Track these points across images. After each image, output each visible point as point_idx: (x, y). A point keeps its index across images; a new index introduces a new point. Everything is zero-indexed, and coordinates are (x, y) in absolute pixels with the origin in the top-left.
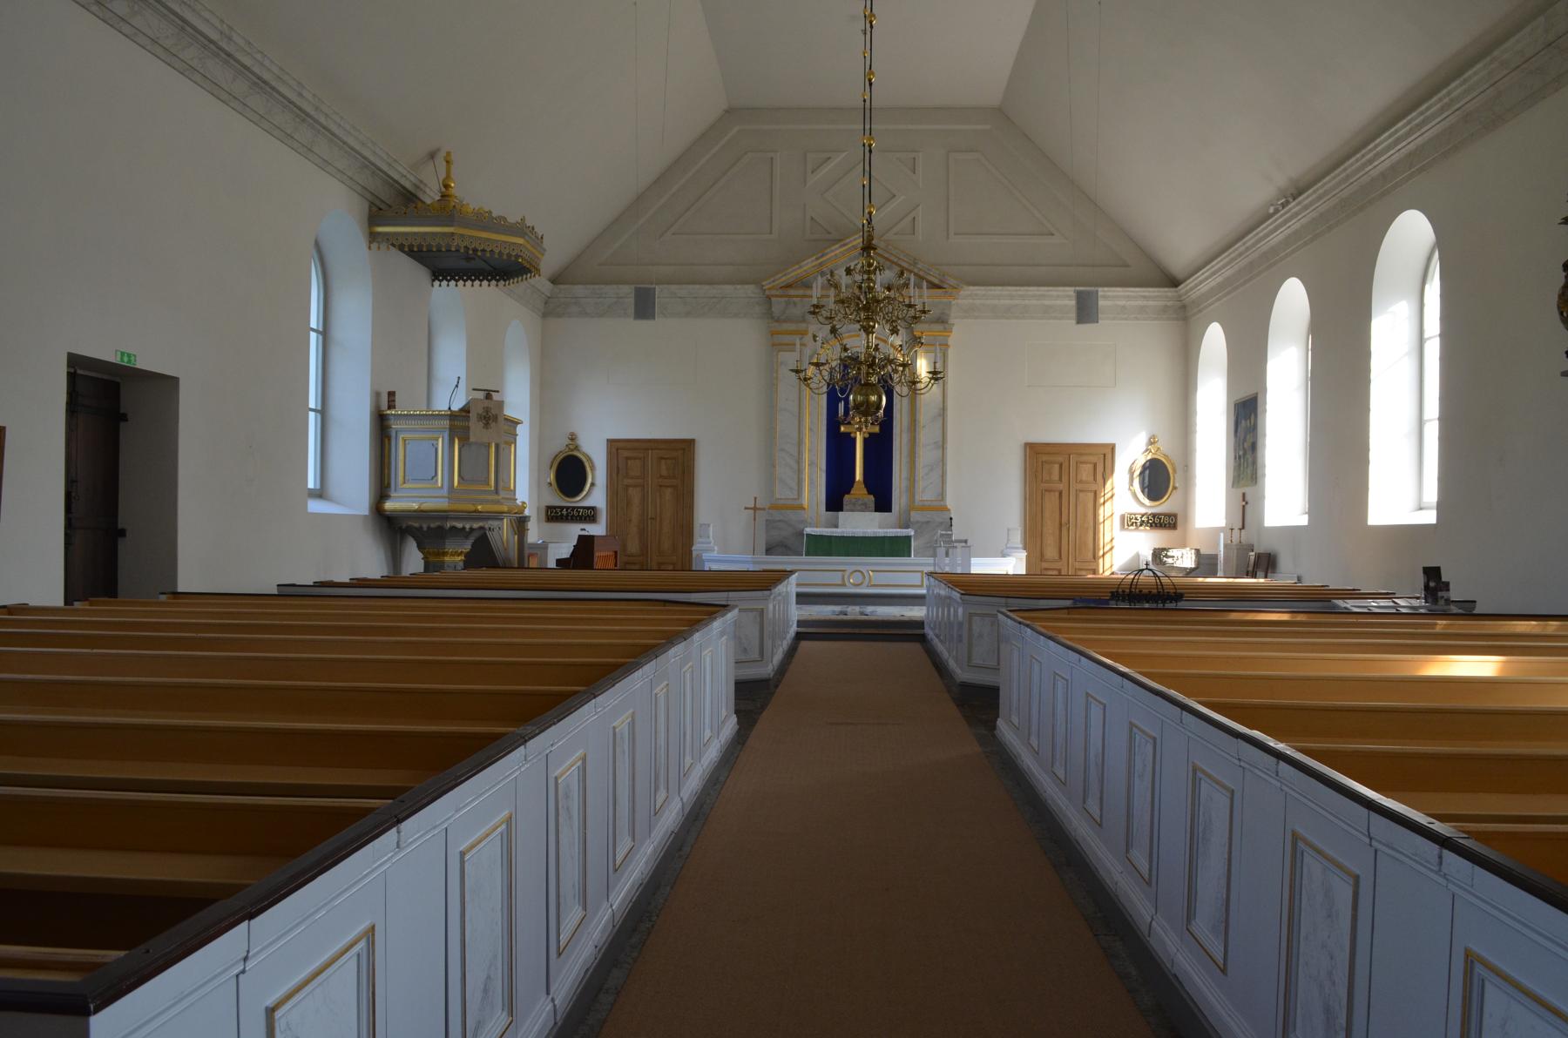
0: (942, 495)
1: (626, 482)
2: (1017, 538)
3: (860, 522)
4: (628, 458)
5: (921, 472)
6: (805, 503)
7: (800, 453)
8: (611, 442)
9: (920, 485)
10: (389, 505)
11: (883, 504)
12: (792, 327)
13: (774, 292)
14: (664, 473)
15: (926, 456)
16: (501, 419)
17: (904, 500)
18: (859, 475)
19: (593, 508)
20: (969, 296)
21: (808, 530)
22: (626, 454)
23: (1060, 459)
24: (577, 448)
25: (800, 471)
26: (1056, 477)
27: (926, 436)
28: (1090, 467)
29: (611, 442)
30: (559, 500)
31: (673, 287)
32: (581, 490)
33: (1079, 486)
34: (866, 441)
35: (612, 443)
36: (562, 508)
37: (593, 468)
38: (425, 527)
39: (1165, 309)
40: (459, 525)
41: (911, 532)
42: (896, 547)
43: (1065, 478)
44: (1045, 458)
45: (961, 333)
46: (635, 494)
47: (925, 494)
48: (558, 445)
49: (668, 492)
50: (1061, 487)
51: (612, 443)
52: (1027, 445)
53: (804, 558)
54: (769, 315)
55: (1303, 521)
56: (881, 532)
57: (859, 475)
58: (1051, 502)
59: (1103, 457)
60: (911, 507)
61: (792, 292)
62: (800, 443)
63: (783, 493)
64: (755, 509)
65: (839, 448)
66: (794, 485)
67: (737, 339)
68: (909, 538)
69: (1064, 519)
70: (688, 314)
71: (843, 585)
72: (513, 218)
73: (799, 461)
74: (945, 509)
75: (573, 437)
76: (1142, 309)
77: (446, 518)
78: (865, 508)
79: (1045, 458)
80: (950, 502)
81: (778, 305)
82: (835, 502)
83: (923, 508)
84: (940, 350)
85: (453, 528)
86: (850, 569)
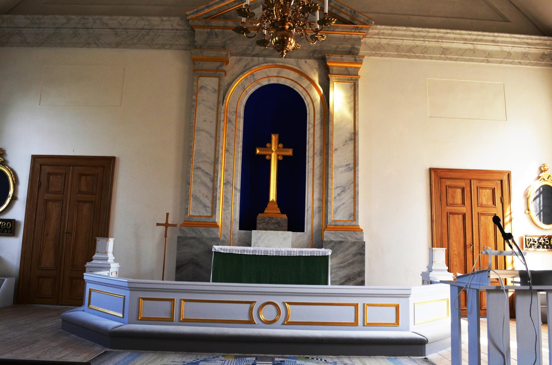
0: (354, 215)
1: (47, 196)
3: (274, 242)
4: (49, 174)
5: (333, 193)
6: (219, 220)
7: (215, 171)
8: (35, 158)
9: (333, 205)
11: (296, 224)
12: (213, 54)
13: (196, 22)
14: (84, 188)
15: (339, 177)
17: (316, 221)
18: (273, 196)
20: (377, 35)
21: (216, 248)
23: (462, 184)
25: (214, 189)
26: (459, 200)
27: (339, 158)
28: (489, 192)
29: (35, 158)
31: (105, 18)
33: (481, 210)
34: (279, 163)
39: (543, 57)
41: (329, 252)
42: (309, 271)
43: (467, 202)
44: (449, 183)
45: (366, 69)
46: (54, 209)
47: (338, 213)
49: (86, 208)
50: (463, 209)
52: (431, 170)
53: (211, 283)
54: (192, 45)
56: (296, 251)
57: (273, 196)
58: (456, 222)
59: (500, 183)
60: (324, 226)
61: (214, 23)
62: (216, 161)
63: (196, 211)
64: (166, 225)
65: (254, 173)
66: (208, 203)
67: (162, 70)
68: (325, 258)
69: (469, 242)
70: (118, 45)
71: (250, 322)
73: (214, 180)
74: (357, 230)
76: (525, 55)
78: (277, 227)
79: (449, 183)
80: (361, 223)
81: (200, 36)
82: (248, 222)
83: (337, 228)
84: (352, 79)
86: (260, 300)
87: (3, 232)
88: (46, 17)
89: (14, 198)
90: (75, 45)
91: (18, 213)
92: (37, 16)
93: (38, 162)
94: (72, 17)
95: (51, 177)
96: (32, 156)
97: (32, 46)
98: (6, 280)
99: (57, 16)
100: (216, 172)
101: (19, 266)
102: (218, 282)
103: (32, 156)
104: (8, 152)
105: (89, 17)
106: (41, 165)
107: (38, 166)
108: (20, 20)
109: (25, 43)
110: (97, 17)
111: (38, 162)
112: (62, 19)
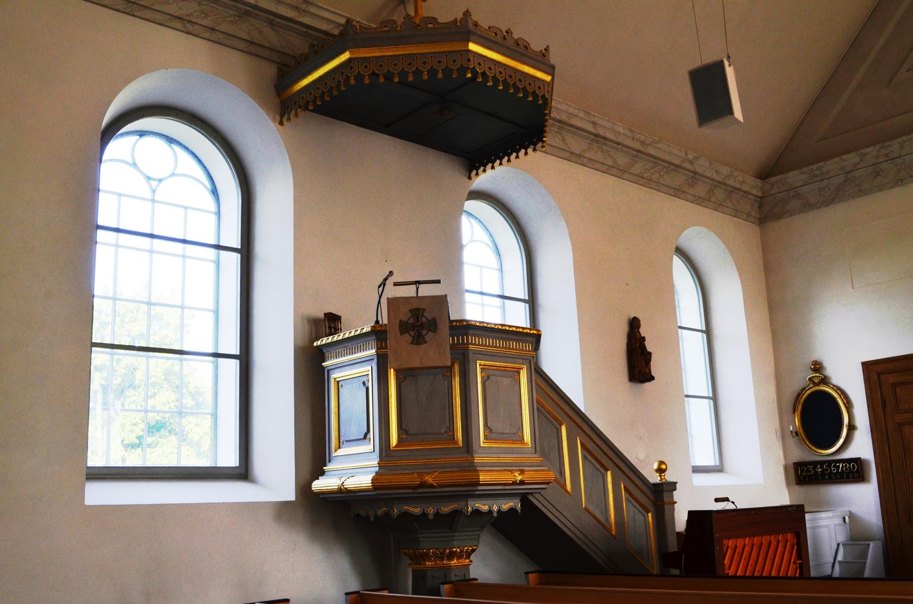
2: (355, 56)
4: (894, 385)
10: (319, 485)
16: (444, 329)
18: (345, 56)
19: (858, 461)
22: (891, 379)
24: (825, 381)
30: (800, 453)
32: (810, 442)
35: (869, 368)
36: (815, 464)
37: (849, 405)
38: (431, 511)
40: (416, 510)
48: (800, 378)
51: (869, 368)
55: (293, 499)
72: (537, 46)
75: (817, 367)
77: (391, 501)
85: (476, 512)
87: (848, 477)
88: (828, 163)
89: (852, 428)
90: (881, 188)
91: (861, 446)
92: (816, 166)
93: (874, 371)
94: (867, 150)
95: (898, 389)
96: (863, 363)
97: (819, 208)
98: (872, 544)
99: (845, 157)
100: (672, 192)
101: (880, 523)
102: (553, 522)
103: (863, 363)
104: (826, 364)
105: (891, 143)
106: (879, 374)
107: (874, 377)
108: (795, 177)
109: (808, 206)
110: (904, 138)
111: (874, 371)
112: (851, 159)
